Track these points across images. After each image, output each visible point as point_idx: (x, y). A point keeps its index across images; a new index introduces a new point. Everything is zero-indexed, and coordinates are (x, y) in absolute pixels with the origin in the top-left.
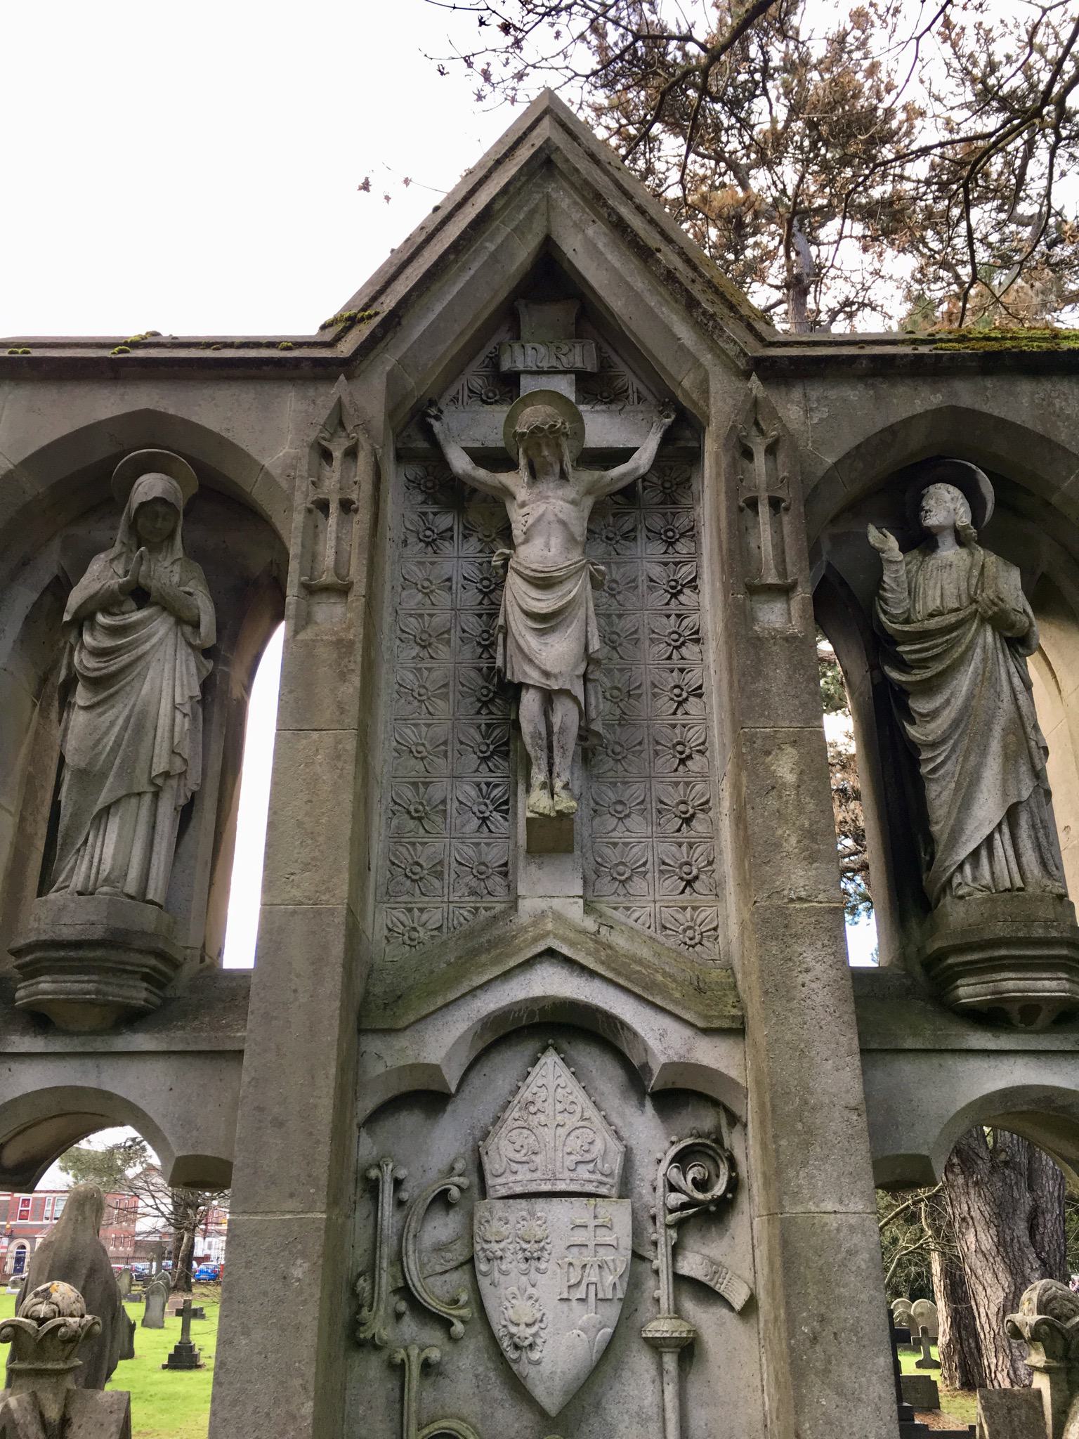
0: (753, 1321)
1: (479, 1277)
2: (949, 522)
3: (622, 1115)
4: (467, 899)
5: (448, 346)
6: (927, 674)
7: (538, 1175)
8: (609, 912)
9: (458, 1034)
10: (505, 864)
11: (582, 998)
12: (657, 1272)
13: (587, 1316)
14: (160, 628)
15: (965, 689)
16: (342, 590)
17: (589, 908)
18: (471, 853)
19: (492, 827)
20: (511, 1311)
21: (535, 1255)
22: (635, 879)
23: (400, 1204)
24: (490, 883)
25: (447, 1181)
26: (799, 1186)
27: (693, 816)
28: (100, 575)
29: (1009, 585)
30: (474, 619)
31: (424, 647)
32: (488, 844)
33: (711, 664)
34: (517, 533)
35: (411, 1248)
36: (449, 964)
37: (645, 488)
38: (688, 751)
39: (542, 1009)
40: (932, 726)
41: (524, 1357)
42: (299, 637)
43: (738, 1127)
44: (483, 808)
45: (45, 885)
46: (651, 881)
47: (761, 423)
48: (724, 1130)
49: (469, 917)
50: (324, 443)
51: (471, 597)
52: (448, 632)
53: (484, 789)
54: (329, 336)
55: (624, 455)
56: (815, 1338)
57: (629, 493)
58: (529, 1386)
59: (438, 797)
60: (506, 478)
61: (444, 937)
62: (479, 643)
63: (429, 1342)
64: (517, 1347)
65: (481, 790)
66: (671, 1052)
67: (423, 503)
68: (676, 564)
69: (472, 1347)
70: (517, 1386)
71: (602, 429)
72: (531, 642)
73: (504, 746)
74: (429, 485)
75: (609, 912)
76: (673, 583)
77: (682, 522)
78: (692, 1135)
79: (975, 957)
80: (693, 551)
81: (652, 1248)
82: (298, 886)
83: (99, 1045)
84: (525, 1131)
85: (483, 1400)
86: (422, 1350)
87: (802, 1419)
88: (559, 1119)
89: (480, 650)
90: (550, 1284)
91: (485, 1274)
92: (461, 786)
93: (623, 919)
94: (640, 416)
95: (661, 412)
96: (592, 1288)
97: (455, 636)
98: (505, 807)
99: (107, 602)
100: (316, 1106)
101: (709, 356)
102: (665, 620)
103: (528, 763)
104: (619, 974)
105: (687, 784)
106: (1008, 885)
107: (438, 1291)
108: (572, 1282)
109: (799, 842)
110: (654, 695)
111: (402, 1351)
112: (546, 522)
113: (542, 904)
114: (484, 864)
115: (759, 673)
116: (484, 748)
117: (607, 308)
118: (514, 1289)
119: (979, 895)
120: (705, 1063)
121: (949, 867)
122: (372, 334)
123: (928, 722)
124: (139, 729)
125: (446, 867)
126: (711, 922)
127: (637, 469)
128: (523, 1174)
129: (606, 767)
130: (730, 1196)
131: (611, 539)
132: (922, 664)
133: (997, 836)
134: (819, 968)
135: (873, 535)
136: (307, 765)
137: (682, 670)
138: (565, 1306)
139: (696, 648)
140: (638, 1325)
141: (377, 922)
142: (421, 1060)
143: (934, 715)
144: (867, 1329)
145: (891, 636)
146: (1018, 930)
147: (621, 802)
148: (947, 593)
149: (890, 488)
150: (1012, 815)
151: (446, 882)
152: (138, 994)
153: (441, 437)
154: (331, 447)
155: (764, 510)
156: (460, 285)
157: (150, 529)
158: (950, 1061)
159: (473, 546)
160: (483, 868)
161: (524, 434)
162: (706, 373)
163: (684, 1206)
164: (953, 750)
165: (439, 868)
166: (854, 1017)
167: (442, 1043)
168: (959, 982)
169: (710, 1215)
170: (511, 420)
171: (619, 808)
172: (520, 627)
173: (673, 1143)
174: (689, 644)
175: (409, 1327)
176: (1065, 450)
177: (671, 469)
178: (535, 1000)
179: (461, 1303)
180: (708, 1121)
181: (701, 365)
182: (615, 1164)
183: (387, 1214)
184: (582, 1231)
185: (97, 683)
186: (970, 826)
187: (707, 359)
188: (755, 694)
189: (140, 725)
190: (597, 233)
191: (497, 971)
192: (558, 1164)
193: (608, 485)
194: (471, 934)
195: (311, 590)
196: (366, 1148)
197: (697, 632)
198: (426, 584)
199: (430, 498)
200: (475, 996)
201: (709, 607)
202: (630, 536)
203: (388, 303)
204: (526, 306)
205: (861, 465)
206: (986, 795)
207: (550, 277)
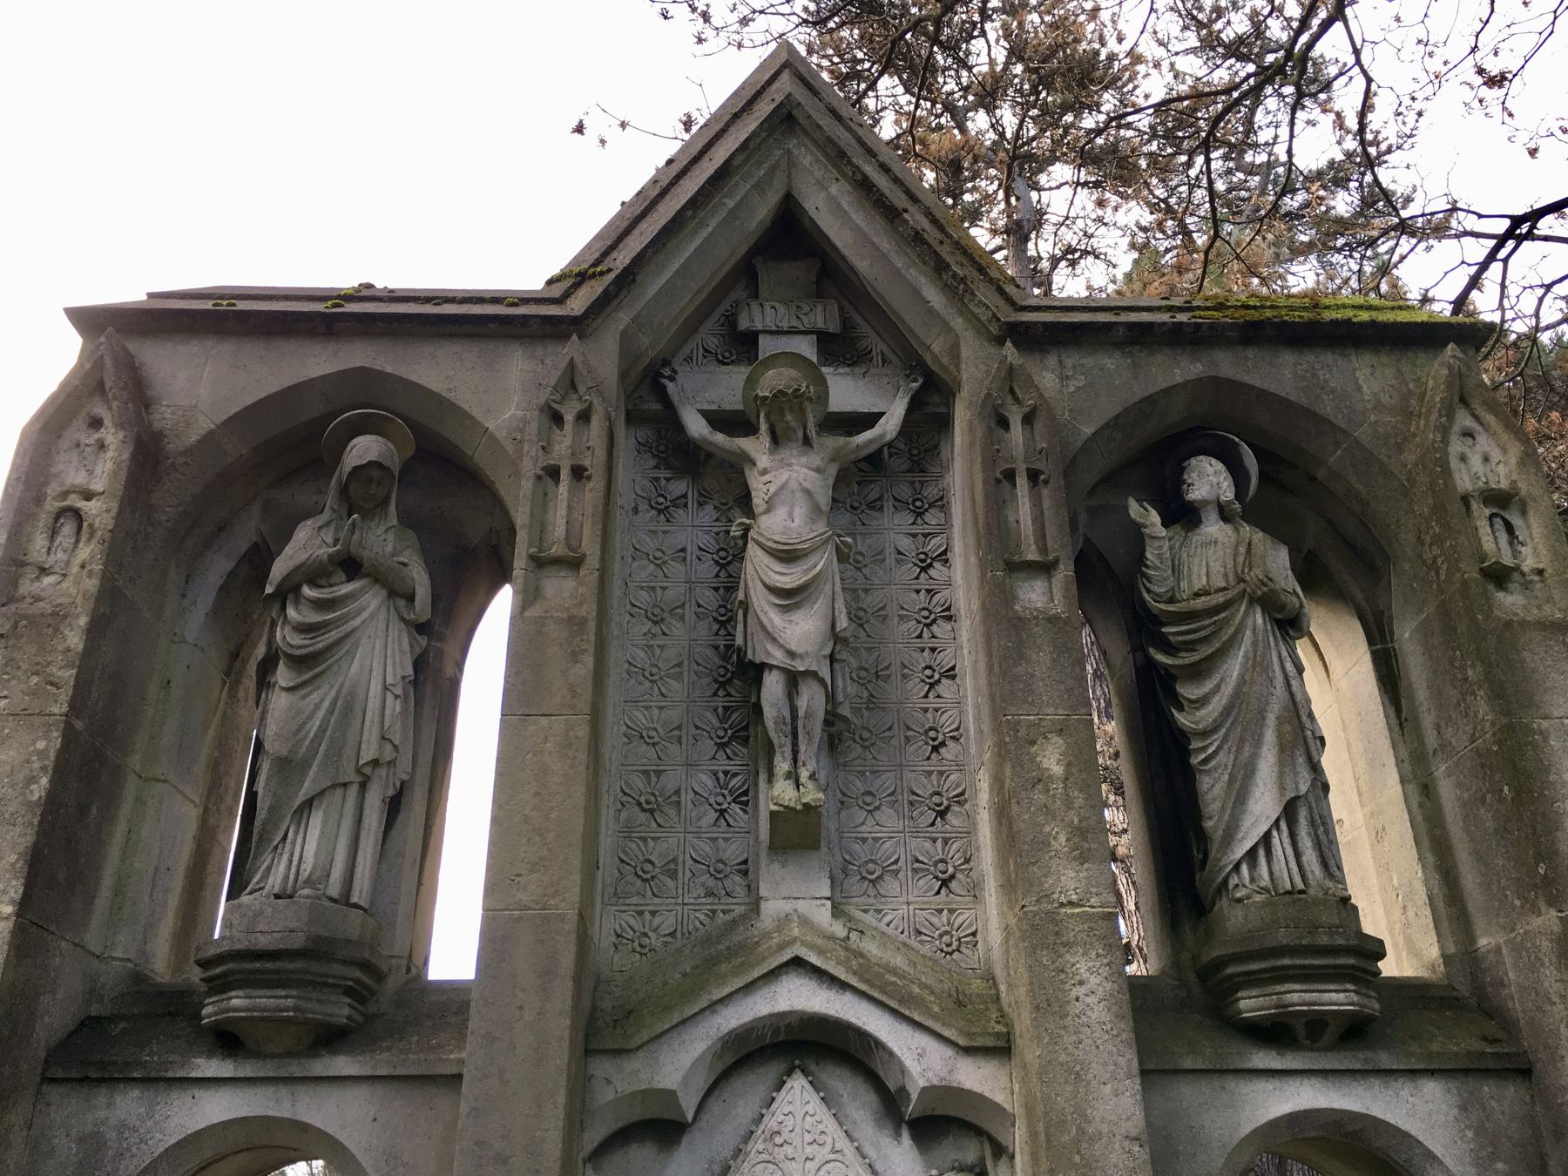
2: (1212, 497)
3: (877, 1146)
5: (685, 303)
6: (1195, 657)
9: (696, 1055)
10: (745, 862)
11: (832, 1012)
15: (1235, 673)
16: (573, 563)
17: (837, 912)
18: (707, 849)
19: (731, 821)
22: (887, 878)
28: (307, 543)
29: (1278, 563)
30: (710, 593)
31: (656, 623)
33: (965, 643)
34: (758, 501)
36: (684, 975)
37: (891, 455)
40: (1203, 712)
42: (527, 614)
44: (720, 799)
50: (555, 406)
51: (707, 569)
52: (682, 606)
54: (557, 291)
55: (871, 420)
57: (874, 461)
59: (671, 787)
60: (745, 444)
61: (679, 944)
62: (715, 619)
65: (718, 779)
66: (930, 1074)
68: (925, 535)
71: (846, 392)
72: (774, 619)
73: (743, 729)
75: (859, 915)
77: (931, 492)
83: (295, 1069)
89: (716, 627)
92: (697, 774)
93: (874, 923)
94: (886, 380)
95: (908, 376)
97: (689, 612)
98: (745, 798)
99: (315, 574)
102: (914, 595)
103: (770, 751)
104: (872, 986)
105: (941, 773)
106: (1289, 887)
110: (905, 676)
112: (788, 489)
113: (787, 907)
115: (1021, 656)
116: (721, 733)
117: (851, 268)
119: (1258, 898)
124: (347, 712)
129: (853, 755)
132: (1190, 646)
133: (1275, 833)
135: (1134, 509)
137: (933, 650)
139: (948, 626)
143: (1203, 701)
147: (869, 793)
149: (1151, 462)
152: (341, 1011)
153: (675, 399)
154: (561, 409)
155: (1022, 482)
157: (362, 495)
159: (708, 515)
161: (766, 398)
164: (1225, 740)
165: (672, 866)
166: (1132, 1035)
168: (1239, 994)
170: (751, 382)
171: (868, 799)
172: (762, 602)
185: (301, 662)
186: (1246, 822)
187: (958, 323)
189: (348, 709)
194: (708, 941)
197: (948, 609)
198: (658, 554)
199: (663, 462)
200: (714, 1012)
201: (962, 582)
202: (876, 506)
203: (622, 259)
207: (790, 234)
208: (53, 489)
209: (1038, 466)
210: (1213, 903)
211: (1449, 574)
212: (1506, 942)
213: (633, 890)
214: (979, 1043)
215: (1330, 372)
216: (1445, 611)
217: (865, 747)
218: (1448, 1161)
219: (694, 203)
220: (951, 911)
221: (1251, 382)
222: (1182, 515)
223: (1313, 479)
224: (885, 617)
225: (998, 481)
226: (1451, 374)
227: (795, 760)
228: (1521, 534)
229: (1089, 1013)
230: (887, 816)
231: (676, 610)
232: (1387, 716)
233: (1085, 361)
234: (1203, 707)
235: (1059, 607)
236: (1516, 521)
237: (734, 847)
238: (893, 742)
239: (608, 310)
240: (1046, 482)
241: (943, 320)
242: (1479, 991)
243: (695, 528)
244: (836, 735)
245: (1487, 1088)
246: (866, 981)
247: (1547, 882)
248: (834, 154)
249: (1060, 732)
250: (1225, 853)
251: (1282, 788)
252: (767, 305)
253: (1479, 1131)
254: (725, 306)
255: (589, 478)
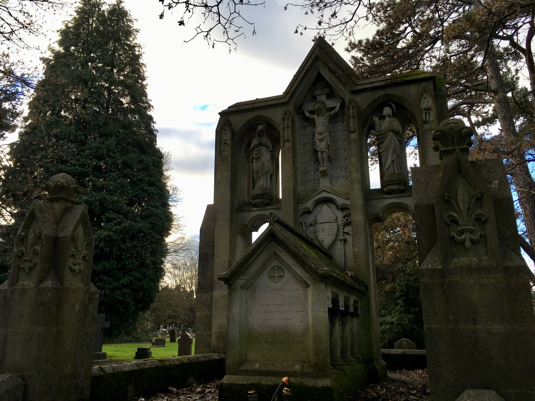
13: (331, 237)
14: (264, 149)
16: (289, 141)
17: (331, 184)
23: (306, 226)
28: (255, 142)
29: (396, 124)
45: (253, 188)
51: (311, 137)
57: (336, 114)
88: (326, 213)
98: (318, 170)
99: (256, 146)
112: (321, 122)
124: (263, 165)
132: (381, 139)
141: (300, 189)
143: (382, 148)
150: (393, 162)
152: (268, 201)
155: (352, 118)
159: (311, 127)
167: (309, 204)
172: (317, 141)
182: (335, 218)
185: (257, 159)
187: (345, 91)
189: (263, 164)
190: (326, 70)
195: (284, 141)
196: (301, 219)
207: (320, 78)
208: (223, 140)
219: (302, 78)
235: (356, 138)
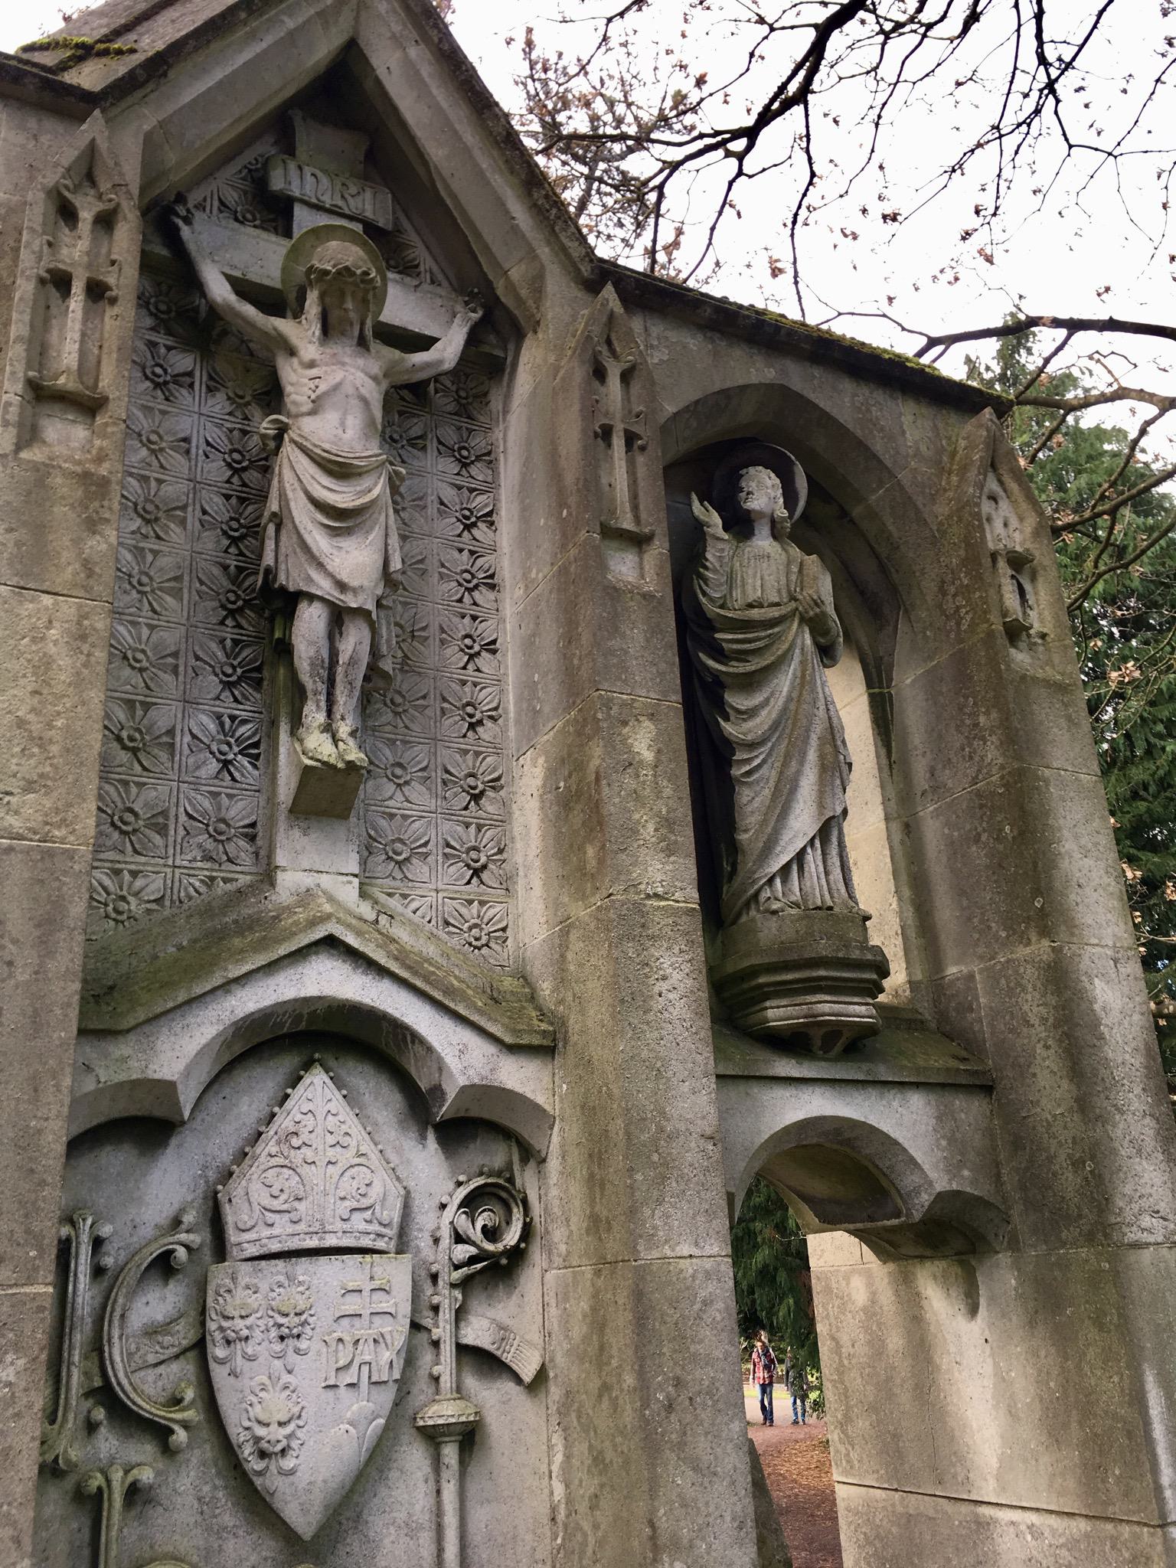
0: (542, 1395)
1: (212, 1365)
2: (768, 511)
3: (399, 1151)
4: (199, 864)
5: (221, 128)
6: (750, 667)
7: (302, 1227)
8: (382, 898)
9: (203, 1041)
10: (253, 825)
11: (367, 1001)
12: (436, 1344)
15: (785, 689)
17: (363, 894)
18: (206, 804)
19: (237, 775)
20: (258, 1408)
21: (295, 1331)
22: (414, 861)
23: (98, 1271)
24: (231, 848)
25: (171, 1239)
26: (655, 1228)
27: (482, 793)
30: (219, 500)
31: (148, 522)
32: (230, 796)
35: (116, 1333)
36: (180, 948)
37: (436, 392)
38: (478, 716)
39: (313, 1014)
40: (750, 724)
41: (273, 1468)
42: (24, 455)
43: (532, 1164)
44: (225, 748)
46: (433, 866)
47: (616, 343)
48: (516, 1167)
49: (203, 889)
50: (66, 194)
51: (216, 470)
52: (184, 508)
53: (227, 725)
55: (426, 342)
56: (670, 1406)
58: (277, 1504)
59: (163, 725)
60: (284, 325)
61: (167, 912)
62: (225, 533)
63: (135, 1458)
64: (263, 1454)
65: (222, 724)
66: (471, 1072)
67: (152, 329)
68: (471, 490)
69: (194, 1460)
70: (257, 1505)
72: (320, 541)
74: (163, 307)
75: (382, 898)
76: (467, 513)
77: (478, 443)
78: (481, 1174)
79: (789, 977)
80: (489, 479)
81: (431, 1314)
82: (16, 813)
84: (285, 1170)
85: (209, 1529)
86: (127, 1472)
87: (656, 1504)
88: (334, 1157)
89: (226, 542)
90: (312, 1366)
91: (222, 1362)
92: (197, 713)
93: (400, 909)
94: (439, 302)
95: (467, 303)
96: (365, 1369)
97: (193, 517)
98: (260, 751)
100: (39, 1132)
101: (547, 250)
102: (456, 554)
103: (298, 694)
104: (416, 973)
105: (477, 754)
106: (819, 903)
107: (149, 1390)
108: (341, 1363)
109: (656, 830)
110: (442, 642)
111: (99, 1475)
112: (332, 395)
113: (308, 880)
114: (223, 821)
115: (616, 629)
116: (230, 671)
117: (421, 155)
118: (265, 1379)
119: (794, 911)
120: (509, 1087)
121: (760, 878)
122: (132, 73)
123: (744, 720)
125: (172, 820)
126: (500, 921)
127: (440, 362)
128: (282, 1226)
129: (383, 719)
130: (523, 1245)
131: (395, 441)
132: (742, 656)
133: (809, 850)
134: (676, 976)
135: (697, 508)
136: (34, 640)
137: (474, 618)
138: (330, 1393)
139: (491, 595)
140: (411, 1412)
142: (152, 1075)
143: (752, 713)
144: (722, 1389)
145: (709, 620)
146: (838, 950)
147: (400, 765)
148: (768, 585)
151: (171, 839)
153: (192, 247)
154: (77, 200)
155: (618, 442)
156: (247, 55)
158: (756, 1089)
159: (219, 404)
160: (223, 826)
161: (326, 272)
162: (542, 267)
163: (472, 1260)
164: (769, 755)
165: (161, 820)
166: (710, 1033)
168: (768, 1004)
169: (496, 1270)
171: (398, 771)
172: (303, 516)
173: (459, 1184)
174: (482, 588)
175: (108, 1443)
176: (880, 461)
177: (467, 376)
178: (307, 1000)
179: (186, 1403)
180: (497, 1155)
181: (536, 257)
182: (392, 1213)
183: (81, 1287)
184: (355, 1297)
186: (786, 836)
187: (544, 252)
188: (611, 652)
191: (261, 960)
192: (329, 1212)
193: (407, 371)
194: (208, 911)
197: (492, 576)
198: (154, 438)
199: (162, 324)
200: (228, 992)
202: (417, 443)
204: (304, 119)
205: (695, 425)
206: (801, 805)
209: (635, 429)
210: (739, 915)
211: (973, 625)
212: (981, 971)
213: (109, 843)
214: (525, 1040)
215: (881, 410)
216: (961, 660)
217: (396, 714)
218: (926, 1167)
220: (482, 903)
221: (817, 401)
222: (740, 524)
223: (844, 514)
224: (425, 571)
225: (596, 435)
226: (988, 437)
227: (330, 713)
228: (1031, 598)
229: (671, 1009)
230: (418, 793)
231: (176, 511)
232: (878, 757)
233: (669, 334)
234: (752, 717)
236: (1028, 587)
237: (241, 805)
238: (429, 712)
239: (130, 100)
240: (643, 449)
241: (529, 244)
242: (942, 1016)
243: (202, 417)
244: (375, 686)
245: (959, 1102)
246: (409, 968)
247: (1042, 914)
248: (418, 10)
249: (651, 717)
250: (761, 866)
251: (821, 806)
252: (308, 171)
253: (951, 1140)
254: (248, 156)
255: (113, 301)
